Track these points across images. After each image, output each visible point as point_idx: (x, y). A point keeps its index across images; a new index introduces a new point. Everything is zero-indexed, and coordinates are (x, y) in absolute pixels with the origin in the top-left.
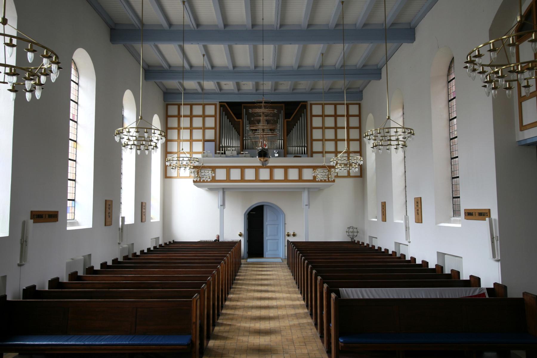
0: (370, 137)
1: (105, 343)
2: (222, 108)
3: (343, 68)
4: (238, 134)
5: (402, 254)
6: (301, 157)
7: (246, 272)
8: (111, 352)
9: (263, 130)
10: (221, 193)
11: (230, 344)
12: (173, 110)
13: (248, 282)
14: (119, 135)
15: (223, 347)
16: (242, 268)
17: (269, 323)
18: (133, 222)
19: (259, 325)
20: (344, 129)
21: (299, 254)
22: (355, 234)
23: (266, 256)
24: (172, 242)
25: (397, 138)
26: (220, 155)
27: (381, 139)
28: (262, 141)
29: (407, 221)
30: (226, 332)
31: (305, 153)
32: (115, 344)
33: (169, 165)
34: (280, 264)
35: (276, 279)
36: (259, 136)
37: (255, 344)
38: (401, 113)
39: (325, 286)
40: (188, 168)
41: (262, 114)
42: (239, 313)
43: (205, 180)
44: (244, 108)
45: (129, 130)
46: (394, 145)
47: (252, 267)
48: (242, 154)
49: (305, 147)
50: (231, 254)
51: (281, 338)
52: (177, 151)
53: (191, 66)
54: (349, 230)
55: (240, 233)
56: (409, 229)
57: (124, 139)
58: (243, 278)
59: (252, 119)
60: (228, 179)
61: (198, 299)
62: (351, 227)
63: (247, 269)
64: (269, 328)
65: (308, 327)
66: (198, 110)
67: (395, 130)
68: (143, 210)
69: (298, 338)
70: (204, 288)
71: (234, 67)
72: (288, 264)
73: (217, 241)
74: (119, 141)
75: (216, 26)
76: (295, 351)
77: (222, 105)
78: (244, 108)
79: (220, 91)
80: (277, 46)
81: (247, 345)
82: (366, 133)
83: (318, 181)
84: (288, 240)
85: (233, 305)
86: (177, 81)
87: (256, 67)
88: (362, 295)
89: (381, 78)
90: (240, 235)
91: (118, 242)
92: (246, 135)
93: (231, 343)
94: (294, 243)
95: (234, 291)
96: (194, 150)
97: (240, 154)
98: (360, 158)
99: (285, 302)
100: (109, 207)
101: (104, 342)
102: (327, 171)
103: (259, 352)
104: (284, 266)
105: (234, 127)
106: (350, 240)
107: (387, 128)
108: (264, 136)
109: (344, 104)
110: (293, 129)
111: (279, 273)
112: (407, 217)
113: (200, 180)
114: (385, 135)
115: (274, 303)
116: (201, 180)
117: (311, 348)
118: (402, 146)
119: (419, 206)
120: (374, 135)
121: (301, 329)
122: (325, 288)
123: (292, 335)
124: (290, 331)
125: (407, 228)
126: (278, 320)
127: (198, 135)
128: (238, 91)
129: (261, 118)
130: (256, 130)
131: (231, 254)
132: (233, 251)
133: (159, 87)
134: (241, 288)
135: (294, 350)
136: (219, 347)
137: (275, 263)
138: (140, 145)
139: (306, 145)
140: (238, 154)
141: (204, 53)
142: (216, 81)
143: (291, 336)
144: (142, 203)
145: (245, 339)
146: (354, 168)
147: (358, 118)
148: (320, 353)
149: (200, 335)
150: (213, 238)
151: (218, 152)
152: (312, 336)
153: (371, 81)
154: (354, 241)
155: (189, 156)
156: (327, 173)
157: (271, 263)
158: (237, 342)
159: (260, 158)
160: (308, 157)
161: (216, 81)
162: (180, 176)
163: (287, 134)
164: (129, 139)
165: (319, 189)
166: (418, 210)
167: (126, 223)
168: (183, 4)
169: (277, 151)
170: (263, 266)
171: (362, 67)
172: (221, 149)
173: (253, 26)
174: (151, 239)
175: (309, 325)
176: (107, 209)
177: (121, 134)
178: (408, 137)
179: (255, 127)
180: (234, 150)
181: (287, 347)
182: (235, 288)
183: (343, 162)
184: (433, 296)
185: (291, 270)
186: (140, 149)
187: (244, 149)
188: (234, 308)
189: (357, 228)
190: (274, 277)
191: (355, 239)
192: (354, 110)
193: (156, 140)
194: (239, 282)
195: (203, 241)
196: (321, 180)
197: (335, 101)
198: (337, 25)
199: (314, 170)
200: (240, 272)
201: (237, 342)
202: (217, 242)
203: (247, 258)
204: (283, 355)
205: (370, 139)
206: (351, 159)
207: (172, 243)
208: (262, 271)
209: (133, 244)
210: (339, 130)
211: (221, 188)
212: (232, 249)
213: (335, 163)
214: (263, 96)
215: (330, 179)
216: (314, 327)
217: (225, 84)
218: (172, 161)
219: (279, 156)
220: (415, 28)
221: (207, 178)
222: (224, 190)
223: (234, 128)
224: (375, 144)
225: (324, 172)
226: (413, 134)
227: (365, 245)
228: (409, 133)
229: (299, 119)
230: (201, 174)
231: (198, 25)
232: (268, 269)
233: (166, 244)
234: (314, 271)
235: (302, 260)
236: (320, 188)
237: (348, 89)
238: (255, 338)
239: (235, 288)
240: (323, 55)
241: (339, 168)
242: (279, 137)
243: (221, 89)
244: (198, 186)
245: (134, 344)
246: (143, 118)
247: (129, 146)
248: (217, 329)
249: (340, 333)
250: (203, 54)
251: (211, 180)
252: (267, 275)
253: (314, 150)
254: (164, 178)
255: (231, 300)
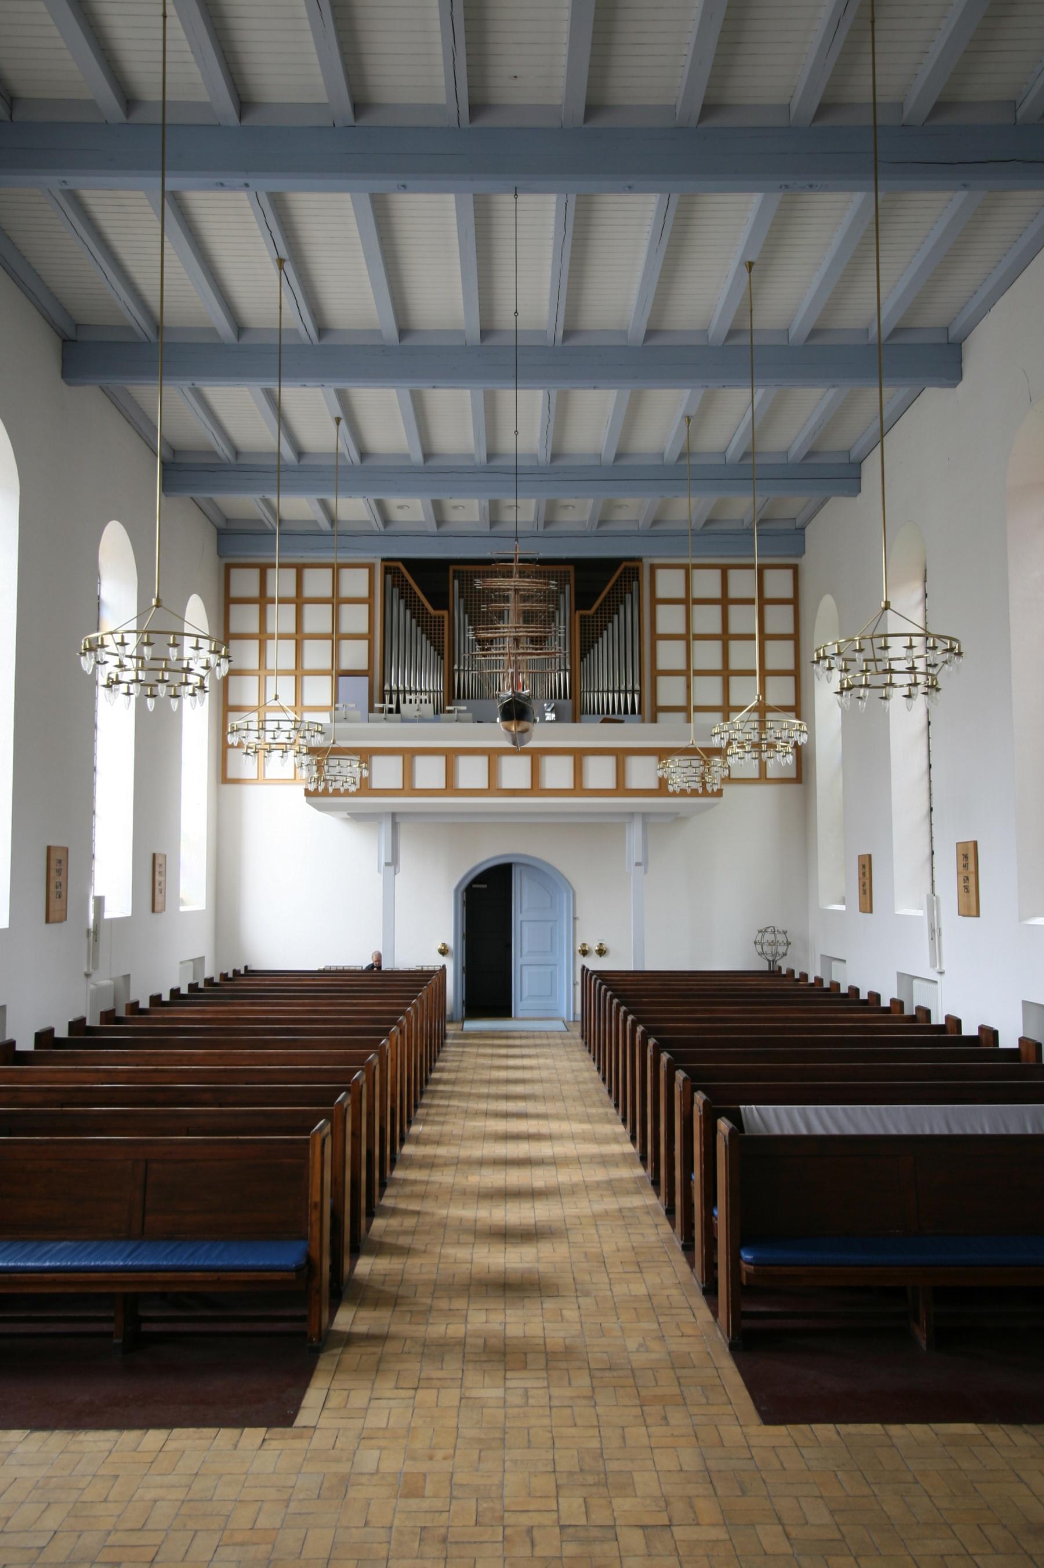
0: (832, 661)
1: (53, 1264)
2: (389, 577)
3: (749, 461)
4: (439, 654)
5: (919, 1009)
6: (622, 722)
7: (461, 1061)
8: (72, 1290)
9: (517, 640)
10: (386, 827)
11: (418, 1268)
12: (245, 583)
13: (466, 1089)
14: (93, 654)
15: (400, 1278)
16: (448, 1049)
17: (533, 1207)
18: (129, 913)
19: (503, 1213)
20: (752, 642)
21: (618, 1006)
22: (781, 950)
23: (520, 1014)
24: (242, 972)
25: (910, 665)
26: (383, 715)
27: (864, 669)
28: (512, 673)
29: (935, 912)
30: (405, 1233)
31: (633, 712)
32: (84, 1267)
33: (236, 745)
34: (561, 1038)
35: (550, 1081)
36: (506, 658)
37: (492, 1268)
38: (919, 594)
39: (700, 1097)
40: (292, 753)
41: (512, 593)
42: (444, 1177)
43: (342, 790)
44: (454, 578)
45: (123, 637)
46: (901, 686)
47: (479, 1046)
48: (450, 712)
49: (633, 692)
50: (418, 1006)
51: (569, 1252)
52: (257, 704)
53: (300, 454)
54: (762, 937)
55: (444, 944)
56: (940, 935)
57: (106, 665)
58: (451, 1076)
59: (484, 608)
60: (406, 788)
61: (328, 1134)
62: (769, 930)
63: (463, 1052)
64: (532, 1221)
65: (648, 1220)
66: (318, 583)
67: (906, 641)
68: (158, 878)
69: (618, 1251)
70: (343, 1105)
71: (427, 456)
72: (582, 1037)
73: (375, 969)
74: (92, 673)
75: (376, 333)
76: (611, 1290)
77: (390, 567)
78: (454, 578)
79: (385, 527)
80: (554, 394)
81: (469, 1271)
82: (822, 650)
83: (674, 792)
84: (584, 967)
85: (424, 1156)
86: (258, 496)
87: (491, 456)
88: (808, 1125)
89: (860, 491)
90: (443, 952)
91: (86, 970)
92: (467, 655)
93: (421, 1265)
94: (600, 974)
95: (427, 1114)
96: (308, 701)
97: (444, 711)
98: (800, 725)
99: (578, 1146)
100: (58, 868)
101: (50, 1262)
102: (702, 763)
103: (504, 1290)
104: (572, 1041)
105: (427, 634)
106: (766, 968)
107: (881, 636)
108: (519, 658)
109: (751, 567)
110: (600, 639)
111: (559, 1064)
112: (935, 898)
113: (326, 789)
114: (877, 657)
115: (545, 1149)
116: (328, 789)
117: (658, 1280)
118: (926, 690)
119: (972, 867)
120: (843, 656)
121: (626, 1226)
122: (698, 1105)
123: (600, 1242)
124: (594, 1231)
125: (935, 932)
126: (559, 1199)
127: (317, 654)
128: (491, 527)
129: (510, 605)
130: (491, 641)
131: (418, 1006)
132: (424, 998)
133: (205, 514)
134: (448, 1106)
135: (608, 1287)
136: (387, 1278)
137: (547, 1034)
138: (156, 683)
139: (637, 687)
140: (437, 714)
141: (340, 414)
142: (372, 498)
143: (599, 1245)
144: (154, 855)
145: (462, 1253)
146: (781, 754)
147: (789, 609)
148: (684, 1295)
149: (332, 1242)
150: (362, 961)
151: (377, 705)
152: (661, 1244)
153: (830, 498)
154: (777, 969)
155: (292, 716)
156: (702, 768)
157: (535, 1033)
158: (439, 1263)
159: (506, 723)
160: (643, 721)
161: (372, 498)
162: (267, 777)
163: (581, 654)
164: (121, 666)
165: (677, 818)
166: (968, 879)
167: (108, 915)
168: (277, 268)
169: (553, 705)
170: (511, 1042)
171: (805, 458)
172: (387, 698)
173: (486, 333)
174: (181, 963)
175: (648, 1213)
176: (53, 873)
177: (99, 650)
178: (945, 662)
179: (491, 633)
180: (426, 702)
181: (587, 1277)
182: (430, 1106)
183: (748, 736)
184: (1014, 1130)
185: (594, 1055)
186: (154, 694)
187: (454, 698)
188: (429, 1164)
189: (785, 933)
190: (544, 1074)
191: (779, 963)
192: (779, 584)
193: (203, 667)
194: (441, 1088)
195: (333, 969)
196: (692, 790)
197: (722, 556)
198: (732, 333)
199: (660, 760)
200: (442, 1061)
201: (439, 1263)
202: (375, 972)
203: (463, 1020)
204: (574, 1299)
205: (832, 668)
206: (771, 729)
207: (242, 975)
208: (507, 1056)
209: (127, 977)
210: (734, 645)
211: (386, 813)
212: (420, 991)
213: (726, 741)
214: (516, 540)
215: (709, 787)
216: (663, 1219)
217: (400, 507)
218: (244, 733)
219: (558, 720)
220: (961, 344)
221: (346, 782)
222: (395, 818)
223: (424, 636)
224: (848, 682)
225: (690, 766)
226: (959, 654)
227: (811, 980)
228: (947, 650)
229: (618, 609)
230: (328, 772)
231: (322, 330)
232: (525, 1051)
233: (224, 977)
234: (665, 1057)
235: (629, 1023)
236: (678, 813)
237: (761, 522)
238: (492, 1249)
239: (430, 1106)
240: (689, 420)
241: (738, 753)
242: (562, 661)
243: (386, 521)
244: (320, 808)
245: (141, 1265)
246: (164, 604)
247: (121, 685)
248: (379, 1224)
249: (741, 1238)
250: (337, 416)
251: (357, 789)
252: (523, 1068)
253: (662, 701)
254: (217, 782)
255: (418, 1140)
